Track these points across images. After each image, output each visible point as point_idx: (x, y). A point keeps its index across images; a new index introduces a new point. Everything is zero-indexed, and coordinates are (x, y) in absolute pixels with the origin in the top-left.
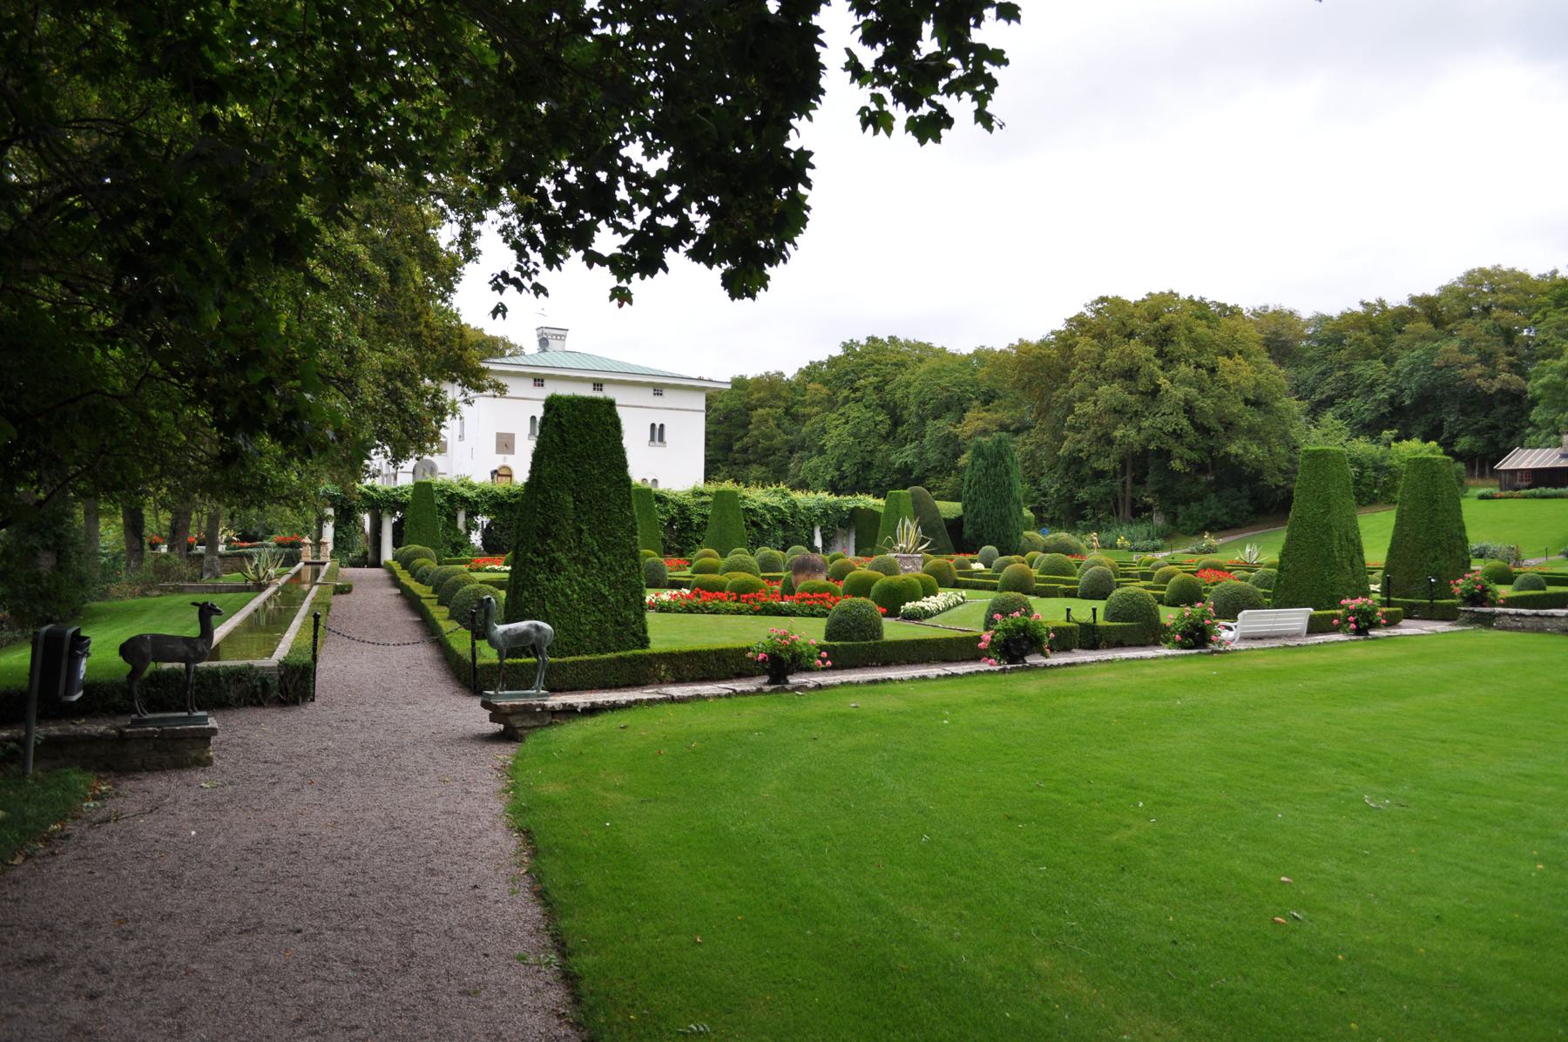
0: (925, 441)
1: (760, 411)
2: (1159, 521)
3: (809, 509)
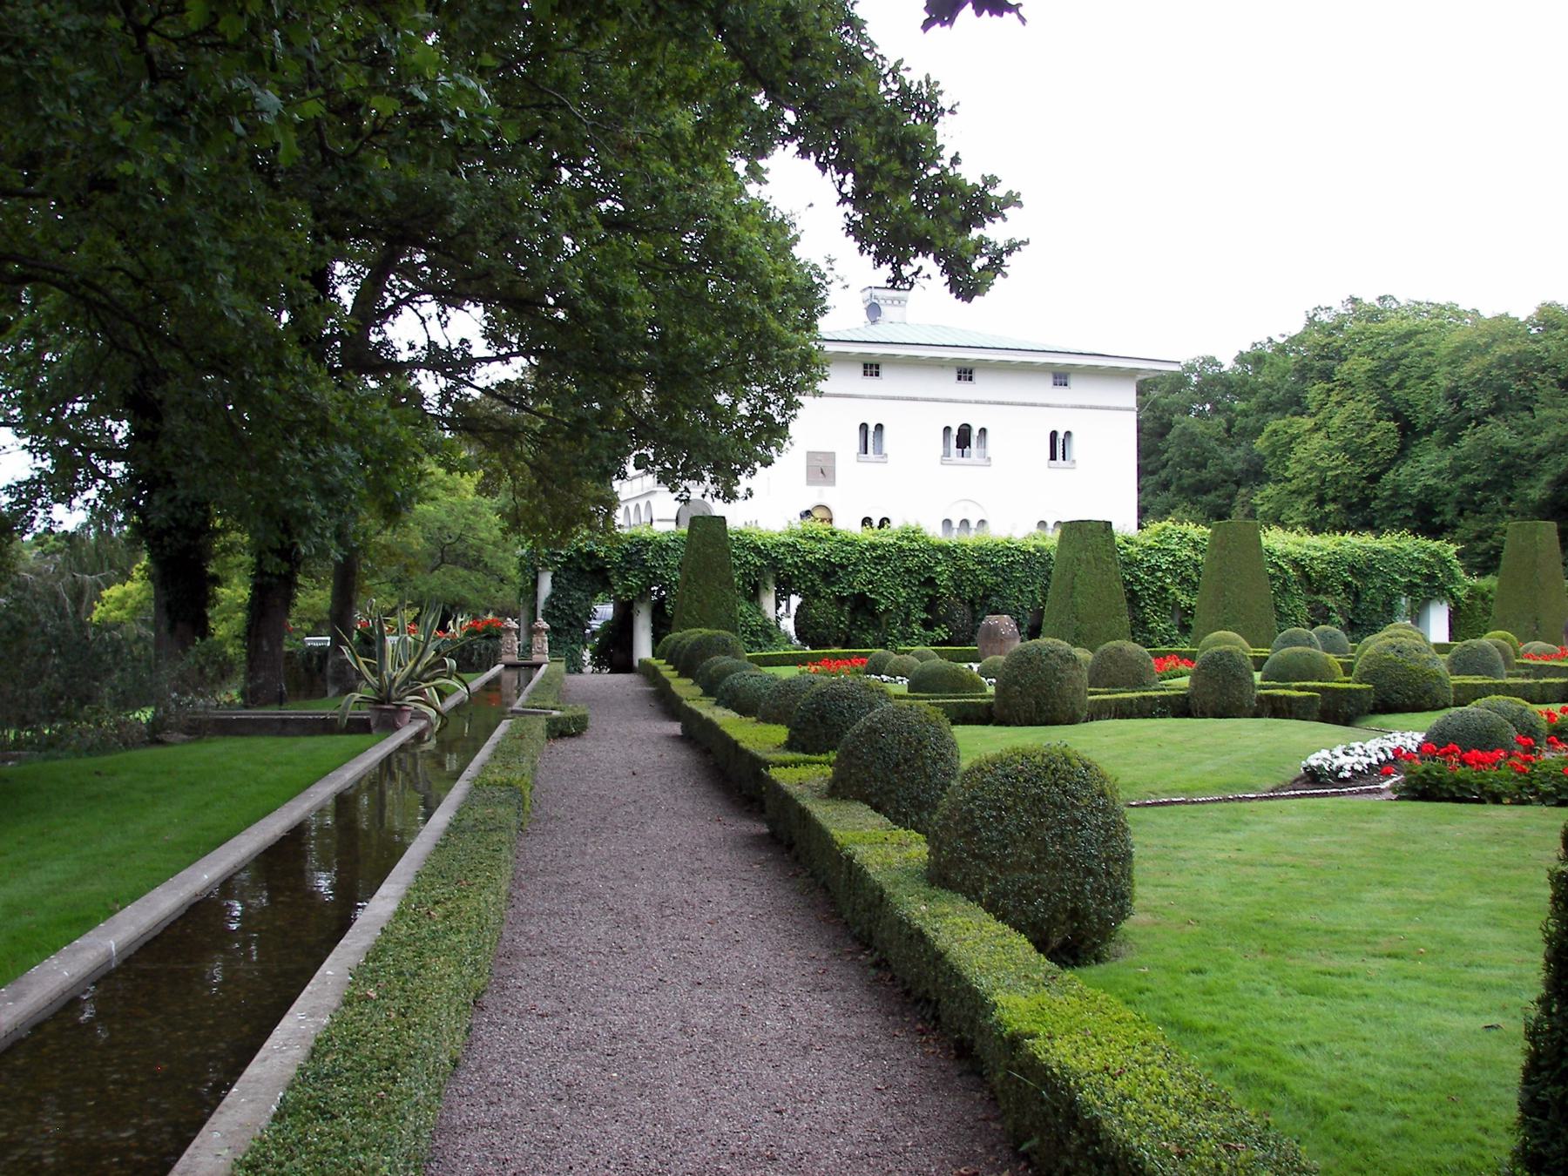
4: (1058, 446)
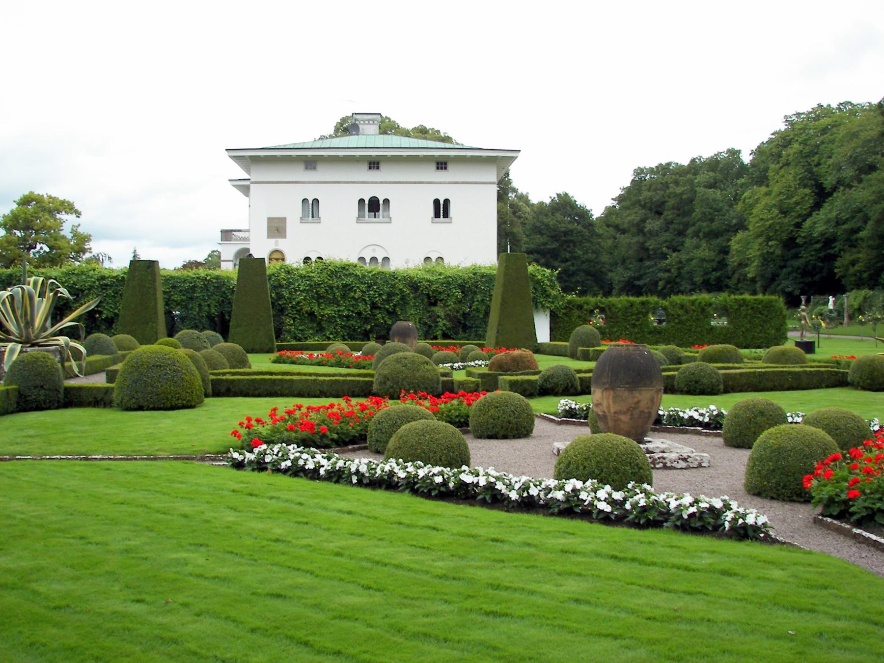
4: (441, 209)
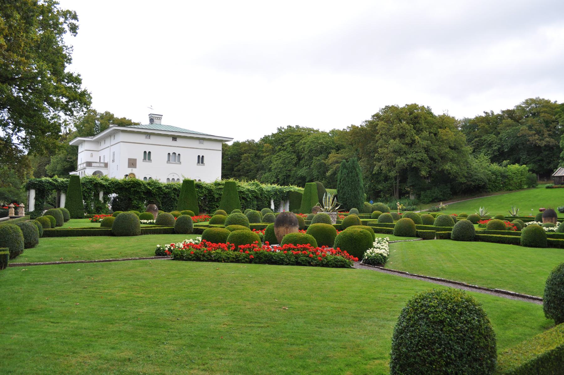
0: (312, 166)
1: (245, 155)
2: (412, 198)
3: (269, 191)
4: (201, 160)
